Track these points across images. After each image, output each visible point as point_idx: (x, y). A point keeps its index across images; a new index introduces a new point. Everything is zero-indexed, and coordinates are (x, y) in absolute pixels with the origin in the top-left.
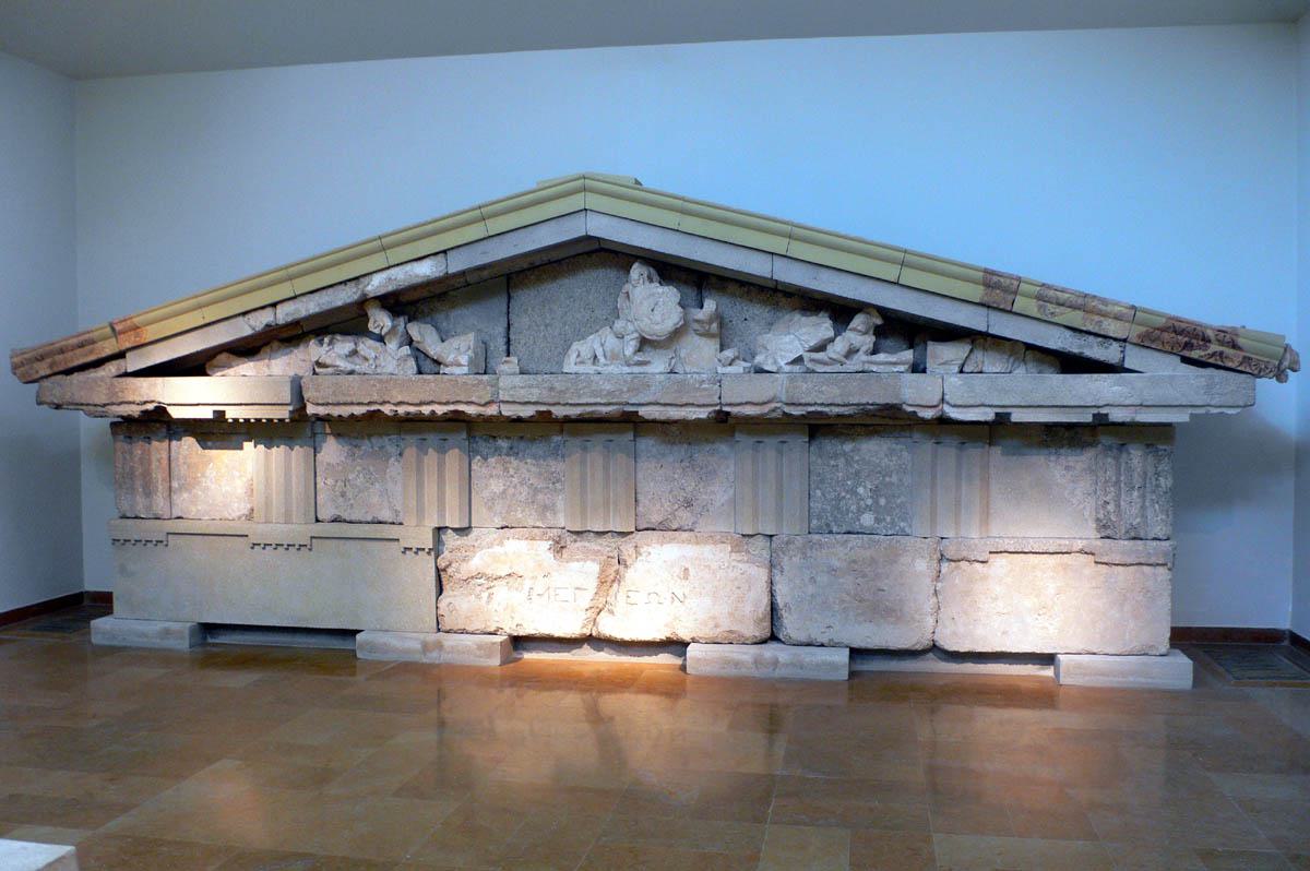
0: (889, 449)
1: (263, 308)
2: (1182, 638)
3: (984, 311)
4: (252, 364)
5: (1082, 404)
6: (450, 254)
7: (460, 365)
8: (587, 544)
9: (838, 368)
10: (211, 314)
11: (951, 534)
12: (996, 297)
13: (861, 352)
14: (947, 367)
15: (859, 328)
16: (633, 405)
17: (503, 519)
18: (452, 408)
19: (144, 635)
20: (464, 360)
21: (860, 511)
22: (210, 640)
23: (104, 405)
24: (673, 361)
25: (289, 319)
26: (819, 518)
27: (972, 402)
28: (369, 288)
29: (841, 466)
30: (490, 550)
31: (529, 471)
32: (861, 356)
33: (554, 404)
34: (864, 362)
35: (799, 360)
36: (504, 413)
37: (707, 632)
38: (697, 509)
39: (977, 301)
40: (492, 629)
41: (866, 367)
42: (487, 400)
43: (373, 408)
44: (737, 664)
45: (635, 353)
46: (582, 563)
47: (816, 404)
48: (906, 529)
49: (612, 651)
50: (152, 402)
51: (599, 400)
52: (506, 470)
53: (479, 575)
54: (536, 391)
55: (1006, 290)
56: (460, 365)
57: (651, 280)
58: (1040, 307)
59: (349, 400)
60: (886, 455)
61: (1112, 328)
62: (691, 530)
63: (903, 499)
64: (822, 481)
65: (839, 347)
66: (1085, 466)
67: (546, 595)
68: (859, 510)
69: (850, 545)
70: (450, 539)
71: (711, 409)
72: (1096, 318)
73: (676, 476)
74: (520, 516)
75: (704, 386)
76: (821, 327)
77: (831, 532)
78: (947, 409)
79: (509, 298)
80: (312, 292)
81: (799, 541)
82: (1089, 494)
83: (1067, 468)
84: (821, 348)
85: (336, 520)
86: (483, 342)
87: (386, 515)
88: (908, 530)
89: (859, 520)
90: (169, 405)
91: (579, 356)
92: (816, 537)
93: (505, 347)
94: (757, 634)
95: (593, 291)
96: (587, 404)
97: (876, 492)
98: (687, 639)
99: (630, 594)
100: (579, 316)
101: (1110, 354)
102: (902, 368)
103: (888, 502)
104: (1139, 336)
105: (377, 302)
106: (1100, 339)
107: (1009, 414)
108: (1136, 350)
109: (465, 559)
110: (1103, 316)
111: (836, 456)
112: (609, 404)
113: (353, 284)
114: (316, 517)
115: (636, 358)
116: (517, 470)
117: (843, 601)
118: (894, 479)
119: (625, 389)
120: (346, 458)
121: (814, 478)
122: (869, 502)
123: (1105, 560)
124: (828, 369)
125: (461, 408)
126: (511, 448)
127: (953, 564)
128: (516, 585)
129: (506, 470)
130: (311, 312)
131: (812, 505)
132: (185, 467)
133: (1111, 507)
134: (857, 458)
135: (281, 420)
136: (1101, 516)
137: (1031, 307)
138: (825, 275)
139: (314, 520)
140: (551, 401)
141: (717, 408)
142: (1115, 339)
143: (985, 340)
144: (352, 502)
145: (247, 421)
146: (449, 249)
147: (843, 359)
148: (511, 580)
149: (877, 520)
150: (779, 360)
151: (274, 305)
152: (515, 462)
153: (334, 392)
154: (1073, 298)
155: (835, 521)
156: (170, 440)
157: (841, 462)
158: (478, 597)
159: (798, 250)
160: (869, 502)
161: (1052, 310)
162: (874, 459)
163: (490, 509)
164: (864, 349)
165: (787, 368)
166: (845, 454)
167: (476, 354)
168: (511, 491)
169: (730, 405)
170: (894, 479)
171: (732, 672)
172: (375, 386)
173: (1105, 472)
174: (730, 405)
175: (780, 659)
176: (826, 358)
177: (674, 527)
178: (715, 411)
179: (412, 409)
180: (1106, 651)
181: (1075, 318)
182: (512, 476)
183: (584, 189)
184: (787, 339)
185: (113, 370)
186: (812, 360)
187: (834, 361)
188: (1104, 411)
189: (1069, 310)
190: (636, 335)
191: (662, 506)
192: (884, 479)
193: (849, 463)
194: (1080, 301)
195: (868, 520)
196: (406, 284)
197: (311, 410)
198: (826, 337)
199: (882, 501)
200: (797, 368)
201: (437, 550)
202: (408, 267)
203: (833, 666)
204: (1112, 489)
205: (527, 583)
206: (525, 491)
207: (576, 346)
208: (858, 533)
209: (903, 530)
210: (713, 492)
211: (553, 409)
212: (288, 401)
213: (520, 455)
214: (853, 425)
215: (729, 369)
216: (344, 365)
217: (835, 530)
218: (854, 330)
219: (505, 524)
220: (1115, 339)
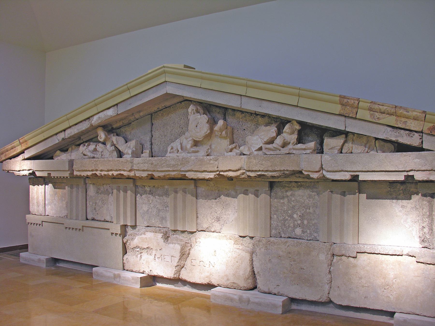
0: (309, 194)
3: (343, 119)
4: (65, 155)
5: (397, 170)
6: (119, 105)
7: (129, 154)
8: (178, 236)
9: (278, 152)
10: (46, 135)
11: (338, 241)
12: (348, 110)
13: (291, 144)
14: (332, 150)
15: (287, 131)
16: (183, 171)
17: (148, 222)
18: (119, 172)
19: (33, 260)
20: (130, 152)
21: (295, 227)
22: (58, 265)
23: (19, 171)
24: (210, 150)
25: (69, 136)
26: (276, 229)
27: (336, 169)
28: (93, 122)
29: (286, 203)
30: (141, 236)
31: (156, 201)
32: (290, 146)
33: (154, 171)
34: (290, 149)
35: (260, 149)
36: (137, 175)
37: (223, 282)
38: (222, 222)
39: (338, 113)
40: (142, 271)
41: (291, 152)
42: (130, 169)
43: (94, 172)
44: (232, 300)
45: (192, 147)
46: (174, 245)
47: (259, 171)
48: (317, 237)
49: (190, 287)
50: (31, 170)
51: (169, 169)
52: (149, 201)
53: (137, 247)
54: (146, 165)
55: (352, 106)
56: (129, 154)
57: (198, 112)
58: (371, 115)
59: (85, 169)
60: (307, 198)
61: (413, 125)
62: (219, 232)
63: (315, 221)
64: (277, 211)
65: (279, 141)
66: (413, 206)
67: (161, 258)
68: (294, 226)
69: (287, 244)
70: (130, 231)
71: (215, 173)
72: (403, 120)
73: (213, 206)
74: (153, 222)
75: (211, 162)
76: (272, 130)
77: (281, 237)
78: (325, 173)
81: (264, 241)
82: (415, 222)
83: (403, 207)
84: (271, 142)
85: (93, 219)
86: (140, 144)
87: (108, 219)
88: (318, 238)
89: (294, 231)
90: (36, 171)
91: (172, 149)
92: (272, 239)
93: (150, 146)
94: (245, 285)
95: (182, 119)
96: (167, 171)
97: (302, 217)
98: (216, 285)
99: (192, 261)
100: (177, 131)
101: (414, 141)
102: (308, 151)
103: (308, 223)
104: (429, 129)
105: (101, 128)
106: (407, 132)
108: (429, 137)
109: (133, 239)
110: (407, 118)
111: (283, 198)
112: (174, 171)
113: (87, 120)
114: (87, 218)
115: (192, 149)
116: (152, 201)
117: (284, 273)
118: (311, 210)
119: (179, 164)
121: (273, 209)
122: (299, 222)
123: (421, 260)
124: (272, 153)
125: (122, 172)
126: (150, 191)
127: (338, 257)
128: (150, 252)
129: (149, 201)
130: (75, 132)
131: (272, 222)
133: (426, 230)
134: (293, 199)
135: (67, 177)
136: (421, 235)
137: (366, 115)
138: (265, 104)
139: (85, 218)
140: (152, 169)
141: (218, 173)
142: (416, 132)
143: (354, 135)
146: (119, 103)
147: (280, 148)
148: (148, 250)
149: (303, 232)
150: (253, 149)
151: (64, 130)
152: (152, 197)
153: (81, 166)
154: (389, 109)
155: (283, 232)
156: (45, 185)
157: (286, 200)
158: (137, 256)
159: (252, 93)
160: (299, 222)
161: (378, 116)
162: (301, 200)
163: (143, 218)
164: (292, 142)
165: (256, 153)
166: (287, 196)
167: (136, 149)
168: (150, 210)
169: (222, 171)
170: (311, 210)
171: (228, 303)
172: (93, 163)
173: (423, 210)
174: (222, 171)
175: (251, 300)
176: (272, 148)
177: (213, 230)
178: (217, 174)
179: (106, 173)
180: (425, 315)
181: (391, 120)
182: (151, 204)
183: (164, 72)
184: (255, 138)
185: (21, 158)
186: (266, 149)
187: (276, 149)
188: (411, 173)
189: (388, 115)
190: (191, 138)
191: (207, 220)
192: (306, 210)
193: (289, 202)
194: (393, 110)
195: (298, 231)
197: (75, 173)
198: (272, 136)
199: (305, 222)
200: (260, 152)
201: (124, 234)
202: (105, 112)
203: (275, 306)
204: (427, 219)
205: (154, 252)
207: (172, 144)
208: (294, 238)
209: (316, 237)
210: (229, 214)
211: (154, 173)
212: (67, 170)
213: (154, 194)
214: (291, 182)
215: (230, 153)
216: (89, 154)
217: (283, 236)
218: (285, 132)
219: (148, 225)
220: (416, 132)
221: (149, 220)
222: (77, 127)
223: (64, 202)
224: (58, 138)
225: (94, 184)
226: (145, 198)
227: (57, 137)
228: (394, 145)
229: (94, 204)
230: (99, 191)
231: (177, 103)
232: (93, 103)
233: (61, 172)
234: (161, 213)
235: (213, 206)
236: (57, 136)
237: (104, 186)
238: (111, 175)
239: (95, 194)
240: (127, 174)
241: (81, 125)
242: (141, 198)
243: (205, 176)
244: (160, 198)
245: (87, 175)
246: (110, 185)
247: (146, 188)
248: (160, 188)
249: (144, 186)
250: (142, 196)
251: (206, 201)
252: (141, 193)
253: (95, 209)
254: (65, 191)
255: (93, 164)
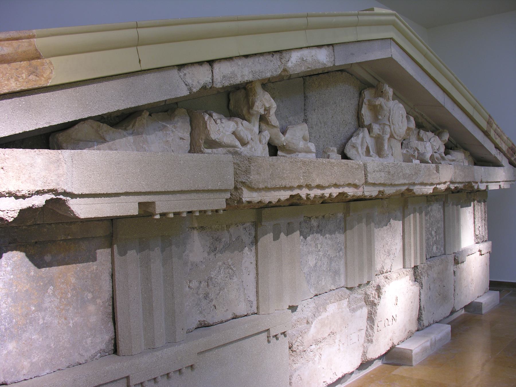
1: (200, 63)
2: (494, 285)
6: (336, 48)
18: (341, 190)
28: (290, 64)
43: (294, 193)
79: (305, 97)
80: (246, 56)
107: (153, 203)
113: (277, 56)
116: (322, 244)
120: (209, 254)
126: (318, 226)
132: (351, 293)
144: (214, 303)
145: (203, 212)
152: (320, 237)
163: (308, 282)
168: (319, 263)
182: (319, 251)
196: (313, 68)
206: (325, 260)
219: (316, 293)
221: (318, 283)
222: (250, 63)
223: (92, 308)
224: (189, 81)
225: (202, 228)
226: (311, 241)
227: (182, 74)
228: (508, 159)
229: (204, 284)
230: (218, 246)
231: (357, 79)
232: (303, 21)
233: (201, 195)
234: (333, 264)
235: (385, 235)
236: (185, 75)
237: (232, 230)
238: (304, 196)
239: (206, 255)
240: (352, 193)
241: (260, 61)
242: (306, 244)
243: (428, 190)
244: (332, 236)
245: (279, 200)
246: (244, 226)
247: (313, 221)
248: (331, 219)
249: (310, 218)
250: (307, 238)
251: (379, 229)
252: (305, 233)
253: (206, 296)
254: (93, 266)
255: (301, 171)
